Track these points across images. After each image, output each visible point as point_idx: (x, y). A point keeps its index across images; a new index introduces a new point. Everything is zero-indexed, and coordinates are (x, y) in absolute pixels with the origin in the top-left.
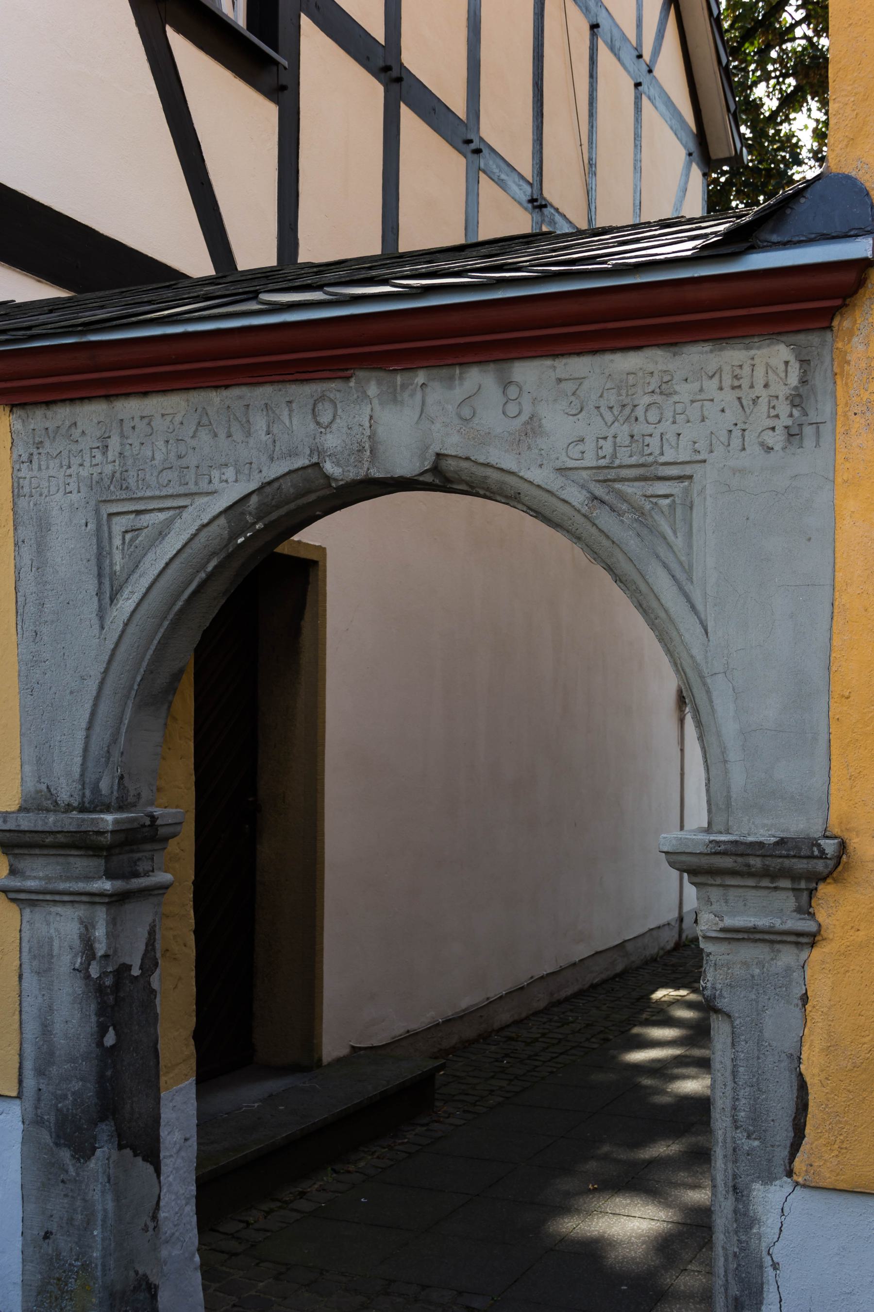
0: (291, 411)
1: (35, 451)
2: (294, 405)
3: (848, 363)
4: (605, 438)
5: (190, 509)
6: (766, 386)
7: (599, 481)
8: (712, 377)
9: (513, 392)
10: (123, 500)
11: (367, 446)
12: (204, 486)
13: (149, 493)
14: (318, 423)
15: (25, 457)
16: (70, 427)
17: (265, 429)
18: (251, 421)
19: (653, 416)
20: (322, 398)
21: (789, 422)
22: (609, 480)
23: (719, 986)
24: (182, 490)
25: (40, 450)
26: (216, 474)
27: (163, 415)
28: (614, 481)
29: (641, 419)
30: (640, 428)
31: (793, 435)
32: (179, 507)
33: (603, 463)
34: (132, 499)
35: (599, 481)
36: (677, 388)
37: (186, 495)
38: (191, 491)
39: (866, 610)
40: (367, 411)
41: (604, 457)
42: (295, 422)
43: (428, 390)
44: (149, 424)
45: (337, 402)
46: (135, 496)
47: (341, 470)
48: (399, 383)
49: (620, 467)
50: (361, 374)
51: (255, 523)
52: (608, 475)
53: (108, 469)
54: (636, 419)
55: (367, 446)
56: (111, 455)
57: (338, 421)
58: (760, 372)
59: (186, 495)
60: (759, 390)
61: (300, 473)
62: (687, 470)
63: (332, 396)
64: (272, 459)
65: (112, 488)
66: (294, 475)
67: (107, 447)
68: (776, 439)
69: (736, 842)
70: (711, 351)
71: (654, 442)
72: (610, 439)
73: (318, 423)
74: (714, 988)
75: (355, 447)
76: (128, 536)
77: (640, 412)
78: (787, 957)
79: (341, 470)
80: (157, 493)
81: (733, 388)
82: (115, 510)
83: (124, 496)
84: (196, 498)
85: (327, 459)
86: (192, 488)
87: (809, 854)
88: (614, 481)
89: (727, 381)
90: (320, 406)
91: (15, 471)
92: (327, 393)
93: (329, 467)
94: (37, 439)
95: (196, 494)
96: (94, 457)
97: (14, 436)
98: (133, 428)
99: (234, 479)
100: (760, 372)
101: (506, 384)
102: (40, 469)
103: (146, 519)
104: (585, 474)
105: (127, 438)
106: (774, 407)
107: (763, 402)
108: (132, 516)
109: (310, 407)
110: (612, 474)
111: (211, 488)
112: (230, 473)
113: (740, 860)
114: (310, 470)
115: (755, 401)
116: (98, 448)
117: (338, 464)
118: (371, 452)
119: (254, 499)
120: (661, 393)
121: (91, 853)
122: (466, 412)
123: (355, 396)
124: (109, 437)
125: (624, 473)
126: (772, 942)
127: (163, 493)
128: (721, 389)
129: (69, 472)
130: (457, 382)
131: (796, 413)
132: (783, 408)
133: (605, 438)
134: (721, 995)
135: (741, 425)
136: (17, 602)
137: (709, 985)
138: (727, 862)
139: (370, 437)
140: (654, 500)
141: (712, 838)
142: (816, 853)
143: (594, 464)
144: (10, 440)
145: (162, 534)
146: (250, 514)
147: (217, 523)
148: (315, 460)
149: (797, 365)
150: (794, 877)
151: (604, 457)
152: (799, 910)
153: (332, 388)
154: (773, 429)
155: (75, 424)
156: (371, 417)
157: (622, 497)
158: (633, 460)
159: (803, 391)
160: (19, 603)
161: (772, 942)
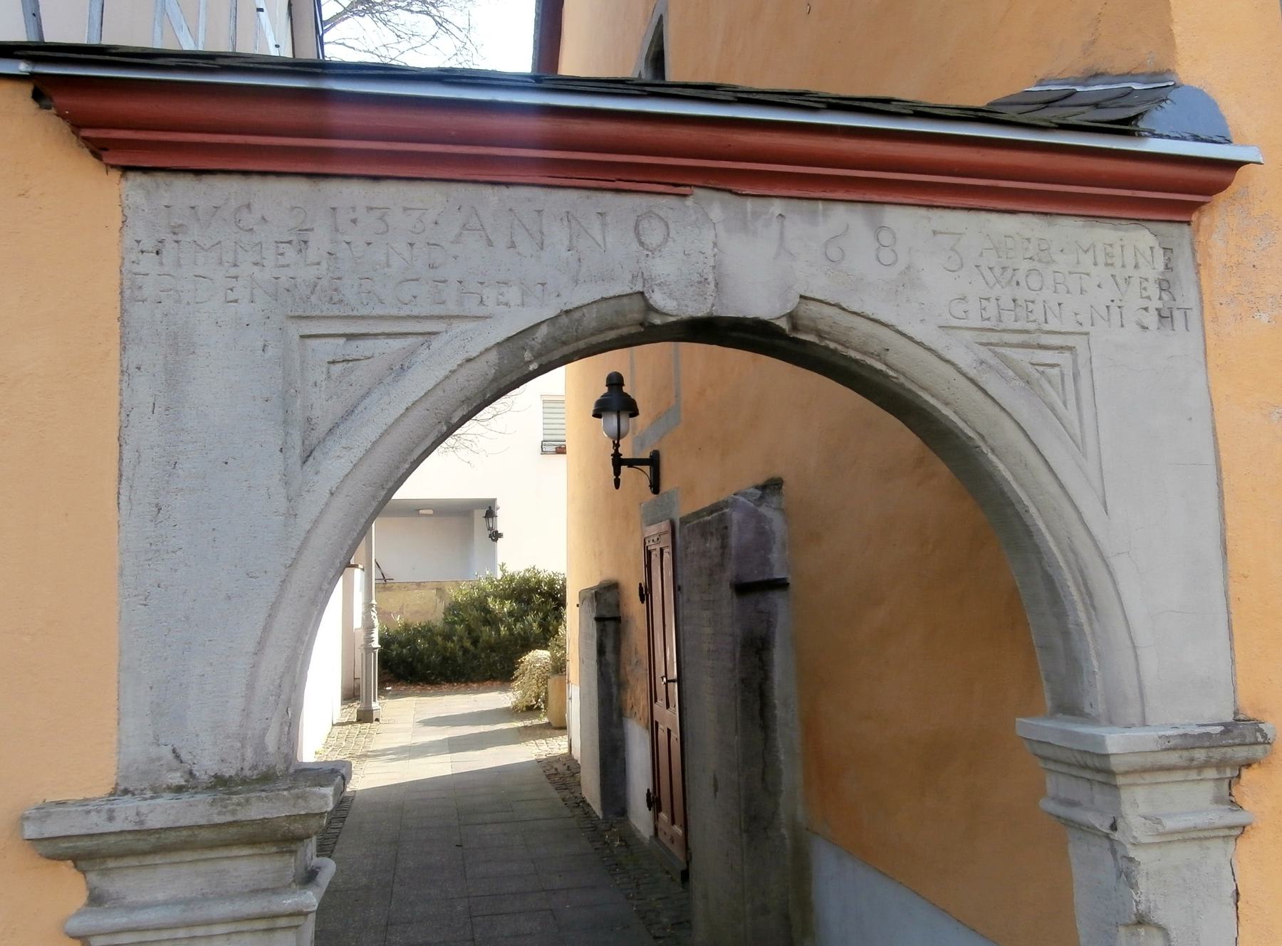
0: (604, 225)
1: (169, 238)
2: (608, 219)
3: (1210, 256)
4: (987, 299)
5: (444, 338)
6: (1136, 266)
7: (981, 344)
8: (1086, 252)
9: (885, 237)
10: (332, 317)
11: (711, 278)
12: (472, 307)
13: (379, 311)
14: (642, 244)
15: (148, 244)
16: (238, 209)
17: (566, 243)
18: (545, 230)
19: (1034, 281)
20: (649, 214)
21: (1159, 305)
22: (991, 344)
23: (1152, 897)
24: (438, 310)
25: (179, 237)
26: (490, 294)
27: (405, 209)
28: (996, 345)
29: (1023, 283)
30: (1022, 294)
31: (1165, 317)
32: (430, 333)
33: (987, 324)
34: (348, 317)
35: (981, 344)
36: (1055, 257)
37: (440, 317)
38: (450, 313)
39: (1254, 490)
40: (709, 236)
41: (988, 319)
42: (609, 239)
43: (787, 223)
44: (381, 218)
45: (670, 222)
46: (355, 313)
47: (675, 303)
48: (749, 210)
49: (1004, 331)
50: (699, 193)
51: (530, 362)
52: (992, 338)
53: (309, 274)
54: (1018, 283)
55: (711, 278)
56: (312, 254)
57: (670, 243)
58: (1129, 253)
59: (440, 317)
60: (1130, 270)
61: (612, 302)
62: (1069, 341)
63: (662, 214)
64: (576, 282)
65: (313, 298)
66: (604, 305)
67: (305, 242)
68: (1151, 319)
69: (1185, 735)
70: (1084, 227)
71: (1038, 310)
72: (993, 300)
73: (642, 244)
74: (1148, 901)
75: (696, 278)
76: (337, 368)
77: (1020, 276)
78: (1217, 852)
79: (675, 303)
80: (394, 312)
81: (1107, 264)
82: (307, 332)
83: (337, 313)
84: (455, 323)
85: (656, 288)
86: (452, 308)
87: (1253, 740)
88: (996, 345)
89: (1101, 259)
90: (644, 224)
91: (127, 264)
92: (656, 210)
93: (658, 299)
94: (176, 221)
95: (458, 317)
96: (282, 254)
97: (127, 212)
98: (354, 221)
99: (519, 302)
100: (1129, 253)
101: (878, 229)
102: (179, 264)
103: (365, 346)
104: (968, 334)
105: (342, 234)
106: (1145, 289)
107: (1135, 282)
108: (342, 341)
109: (632, 224)
110: (994, 338)
111: (481, 311)
112: (513, 294)
113: (1185, 754)
114: (625, 300)
115: (1128, 280)
116: (290, 242)
117: (670, 295)
118: (717, 285)
119: (544, 330)
120: (1040, 261)
121: (274, 849)
122: (834, 253)
123: (693, 218)
124: (312, 230)
125: (1008, 338)
126: (1200, 839)
127: (402, 313)
128: (1095, 264)
129: (233, 271)
130: (821, 219)
131: (1165, 296)
132: (1153, 290)
133: (987, 299)
134: (1156, 907)
135: (1117, 303)
136: (121, 459)
137: (1143, 898)
138: (1173, 758)
139: (714, 267)
140: (1041, 369)
141: (1161, 733)
142: (1260, 739)
143: (979, 324)
144: (119, 218)
145: (400, 369)
146: (532, 349)
147: (484, 358)
148: (639, 288)
149: (1162, 251)
150: (1220, 765)
151: (988, 319)
152: (1218, 800)
153: (665, 205)
154: (1146, 309)
155: (248, 206)
156: (715, 244)
157: (1004, 359)
158: (1018, 326)
159: (1168, 276)
160: (126, 461)
161: (1200, 839)
